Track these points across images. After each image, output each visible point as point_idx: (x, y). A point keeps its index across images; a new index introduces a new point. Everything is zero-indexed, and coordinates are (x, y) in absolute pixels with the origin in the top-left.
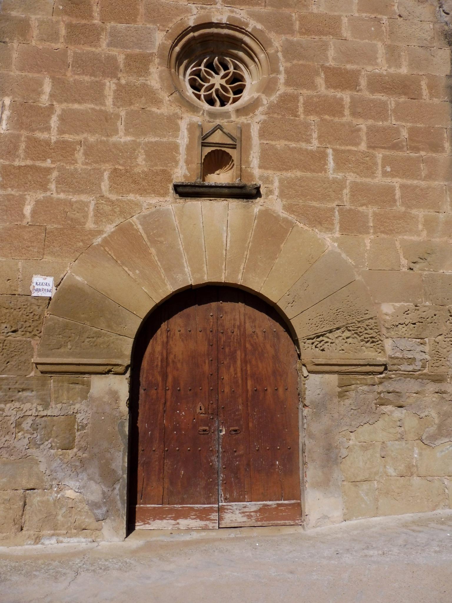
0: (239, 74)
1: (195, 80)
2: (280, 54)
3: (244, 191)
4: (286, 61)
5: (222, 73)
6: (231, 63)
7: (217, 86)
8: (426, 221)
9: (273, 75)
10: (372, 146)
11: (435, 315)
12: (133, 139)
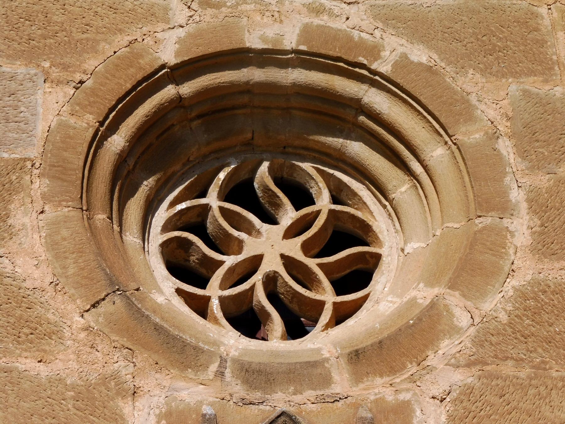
0: (353, 217)
1: (186, 244)
2: (505, 147)
4: (532, 168)
5: (289, 215)
6: (319, 178)
7: (272, 264)
9: (487, 221)
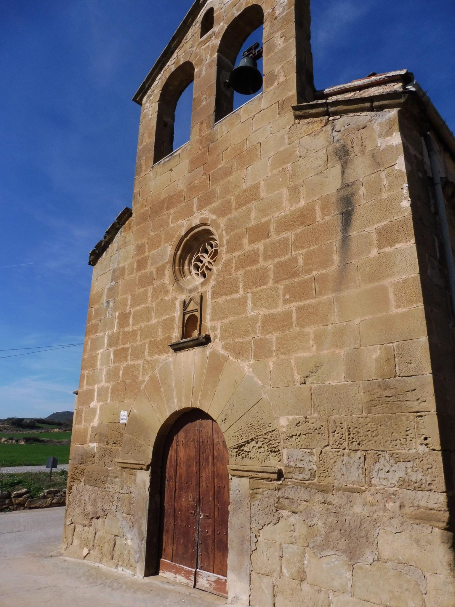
3: (199, 341)
8: (316, 336)
10: (277, 282)
11: (322, 426)
12: (150, 323)
